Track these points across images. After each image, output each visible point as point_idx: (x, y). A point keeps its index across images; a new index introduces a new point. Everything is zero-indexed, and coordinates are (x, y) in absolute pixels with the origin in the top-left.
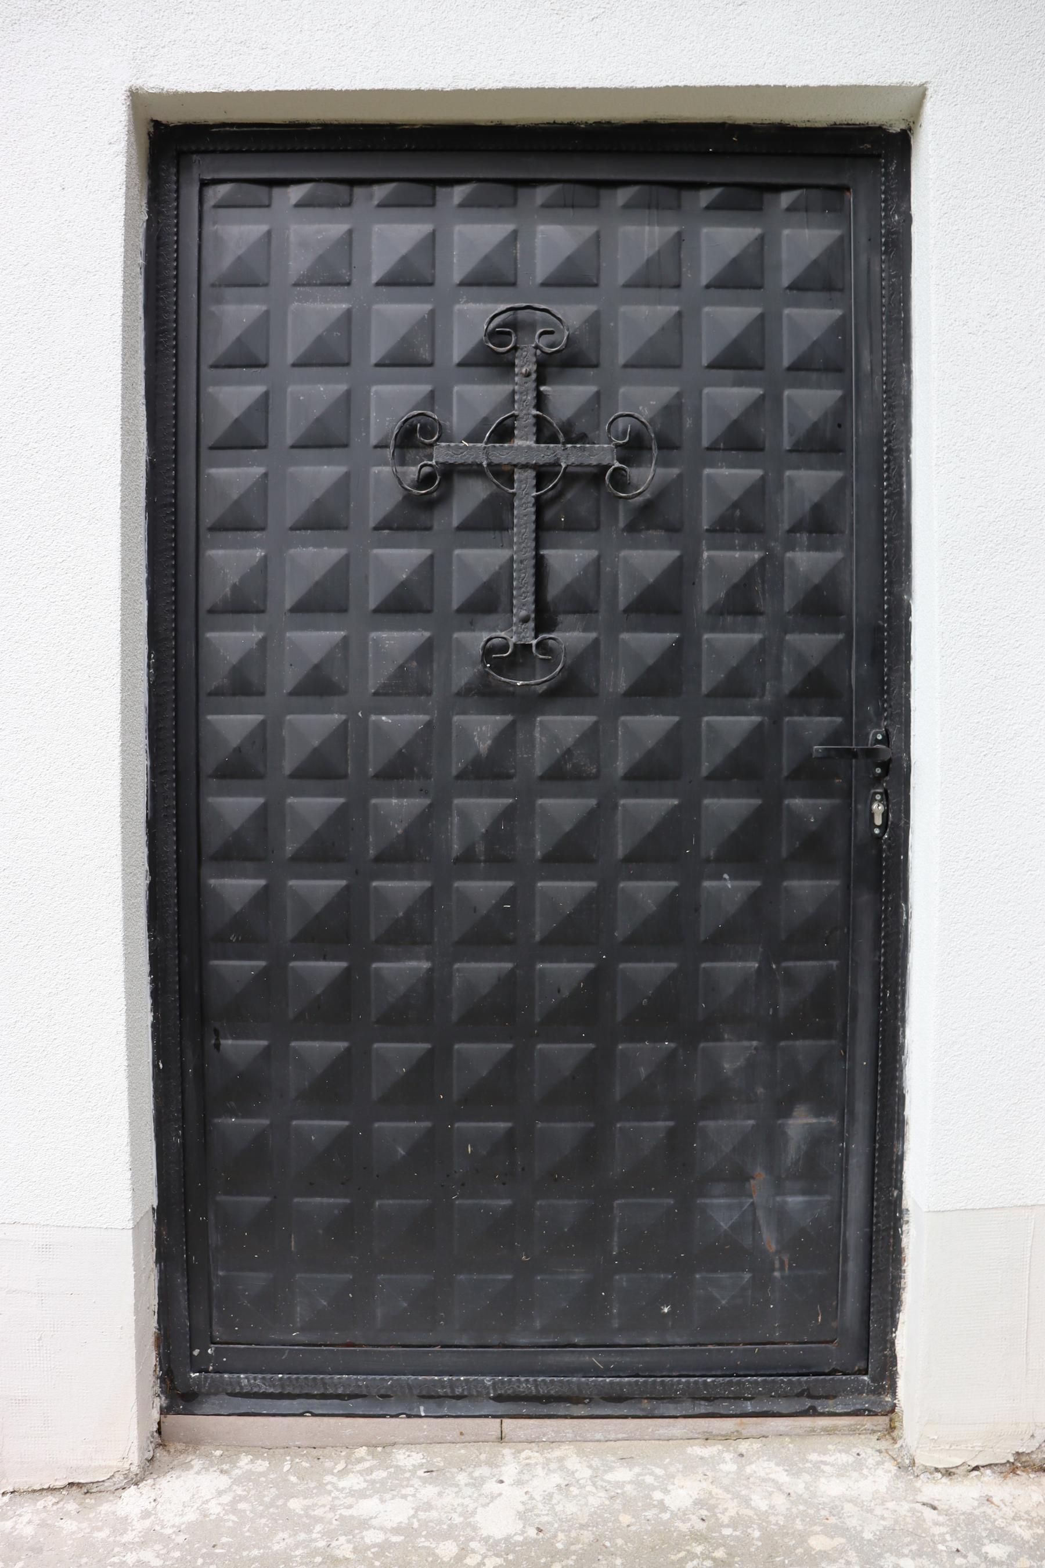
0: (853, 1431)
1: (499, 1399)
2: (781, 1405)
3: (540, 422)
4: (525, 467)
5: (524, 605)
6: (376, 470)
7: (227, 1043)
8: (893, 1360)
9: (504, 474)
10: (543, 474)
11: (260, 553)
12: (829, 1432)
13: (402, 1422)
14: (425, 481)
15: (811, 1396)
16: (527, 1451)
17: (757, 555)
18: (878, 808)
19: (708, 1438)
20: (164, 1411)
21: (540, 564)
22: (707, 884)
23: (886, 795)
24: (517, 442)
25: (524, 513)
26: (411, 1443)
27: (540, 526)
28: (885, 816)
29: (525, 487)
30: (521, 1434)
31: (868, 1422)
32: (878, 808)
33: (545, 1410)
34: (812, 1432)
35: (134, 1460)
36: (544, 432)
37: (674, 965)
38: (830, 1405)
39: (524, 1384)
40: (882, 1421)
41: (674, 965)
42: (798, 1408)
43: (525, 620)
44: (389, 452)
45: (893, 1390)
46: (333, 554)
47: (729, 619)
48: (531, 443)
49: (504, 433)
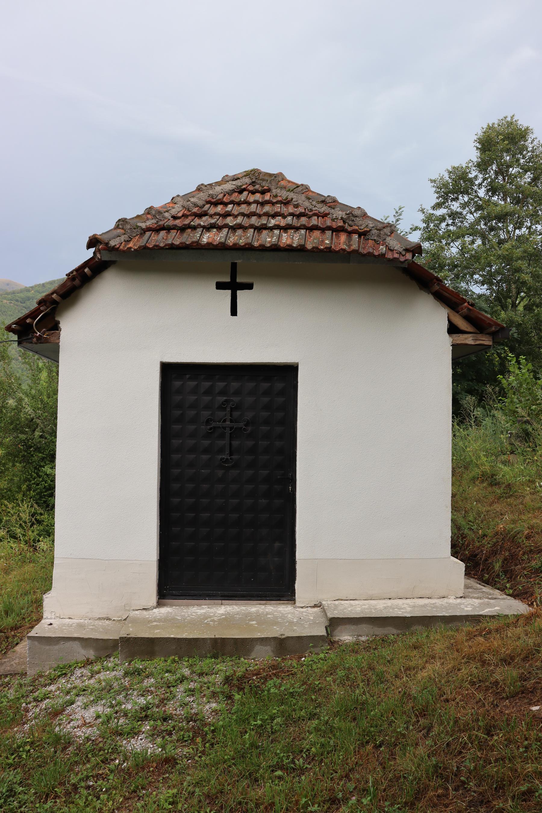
0: (287, 604)
1: (222, 596)
2: (274, 598)
3: (231, 419)
4: (228, 427)
5: (227, 452)
6: (202, 427)
7: (173, 529)
8: (295, 590)
9: (224, 428)
10: (231, 428)
11: (181, 441)
12: (283, 604)
13: (203, 601)
14: (211, 429)
15: (279, 597)
16: (280, 218)
17: (269, 443)
18: (290, 488)
19: (260, 604)
20: (159, 599)
21: (231, 445)
22: (260, 501)
23: (292, 485)
24: (227, 423)
25: (228, 435)
26: (205, 605)
27: (231, 437)
28: (291, 489)
29: (228, 431)
30: (225, 603)
31: (290, 602)
32: (290, 488)
33: (230, 599)
34: (280, 604)
35: (155, 604)
36: (231, 421)
37: (254, 486)
38: (283, 599)
39: (226, 593)
40: (293, 602)
41: (254, 486)
42: (277, 599)
43: (228, 454)
44: (204, 424)
45: (295, 596)
46: (194, 442)
47: (172, 227)
48: (229, 423)
49: (225, 421)
